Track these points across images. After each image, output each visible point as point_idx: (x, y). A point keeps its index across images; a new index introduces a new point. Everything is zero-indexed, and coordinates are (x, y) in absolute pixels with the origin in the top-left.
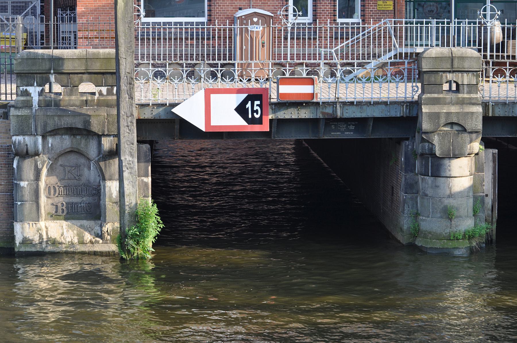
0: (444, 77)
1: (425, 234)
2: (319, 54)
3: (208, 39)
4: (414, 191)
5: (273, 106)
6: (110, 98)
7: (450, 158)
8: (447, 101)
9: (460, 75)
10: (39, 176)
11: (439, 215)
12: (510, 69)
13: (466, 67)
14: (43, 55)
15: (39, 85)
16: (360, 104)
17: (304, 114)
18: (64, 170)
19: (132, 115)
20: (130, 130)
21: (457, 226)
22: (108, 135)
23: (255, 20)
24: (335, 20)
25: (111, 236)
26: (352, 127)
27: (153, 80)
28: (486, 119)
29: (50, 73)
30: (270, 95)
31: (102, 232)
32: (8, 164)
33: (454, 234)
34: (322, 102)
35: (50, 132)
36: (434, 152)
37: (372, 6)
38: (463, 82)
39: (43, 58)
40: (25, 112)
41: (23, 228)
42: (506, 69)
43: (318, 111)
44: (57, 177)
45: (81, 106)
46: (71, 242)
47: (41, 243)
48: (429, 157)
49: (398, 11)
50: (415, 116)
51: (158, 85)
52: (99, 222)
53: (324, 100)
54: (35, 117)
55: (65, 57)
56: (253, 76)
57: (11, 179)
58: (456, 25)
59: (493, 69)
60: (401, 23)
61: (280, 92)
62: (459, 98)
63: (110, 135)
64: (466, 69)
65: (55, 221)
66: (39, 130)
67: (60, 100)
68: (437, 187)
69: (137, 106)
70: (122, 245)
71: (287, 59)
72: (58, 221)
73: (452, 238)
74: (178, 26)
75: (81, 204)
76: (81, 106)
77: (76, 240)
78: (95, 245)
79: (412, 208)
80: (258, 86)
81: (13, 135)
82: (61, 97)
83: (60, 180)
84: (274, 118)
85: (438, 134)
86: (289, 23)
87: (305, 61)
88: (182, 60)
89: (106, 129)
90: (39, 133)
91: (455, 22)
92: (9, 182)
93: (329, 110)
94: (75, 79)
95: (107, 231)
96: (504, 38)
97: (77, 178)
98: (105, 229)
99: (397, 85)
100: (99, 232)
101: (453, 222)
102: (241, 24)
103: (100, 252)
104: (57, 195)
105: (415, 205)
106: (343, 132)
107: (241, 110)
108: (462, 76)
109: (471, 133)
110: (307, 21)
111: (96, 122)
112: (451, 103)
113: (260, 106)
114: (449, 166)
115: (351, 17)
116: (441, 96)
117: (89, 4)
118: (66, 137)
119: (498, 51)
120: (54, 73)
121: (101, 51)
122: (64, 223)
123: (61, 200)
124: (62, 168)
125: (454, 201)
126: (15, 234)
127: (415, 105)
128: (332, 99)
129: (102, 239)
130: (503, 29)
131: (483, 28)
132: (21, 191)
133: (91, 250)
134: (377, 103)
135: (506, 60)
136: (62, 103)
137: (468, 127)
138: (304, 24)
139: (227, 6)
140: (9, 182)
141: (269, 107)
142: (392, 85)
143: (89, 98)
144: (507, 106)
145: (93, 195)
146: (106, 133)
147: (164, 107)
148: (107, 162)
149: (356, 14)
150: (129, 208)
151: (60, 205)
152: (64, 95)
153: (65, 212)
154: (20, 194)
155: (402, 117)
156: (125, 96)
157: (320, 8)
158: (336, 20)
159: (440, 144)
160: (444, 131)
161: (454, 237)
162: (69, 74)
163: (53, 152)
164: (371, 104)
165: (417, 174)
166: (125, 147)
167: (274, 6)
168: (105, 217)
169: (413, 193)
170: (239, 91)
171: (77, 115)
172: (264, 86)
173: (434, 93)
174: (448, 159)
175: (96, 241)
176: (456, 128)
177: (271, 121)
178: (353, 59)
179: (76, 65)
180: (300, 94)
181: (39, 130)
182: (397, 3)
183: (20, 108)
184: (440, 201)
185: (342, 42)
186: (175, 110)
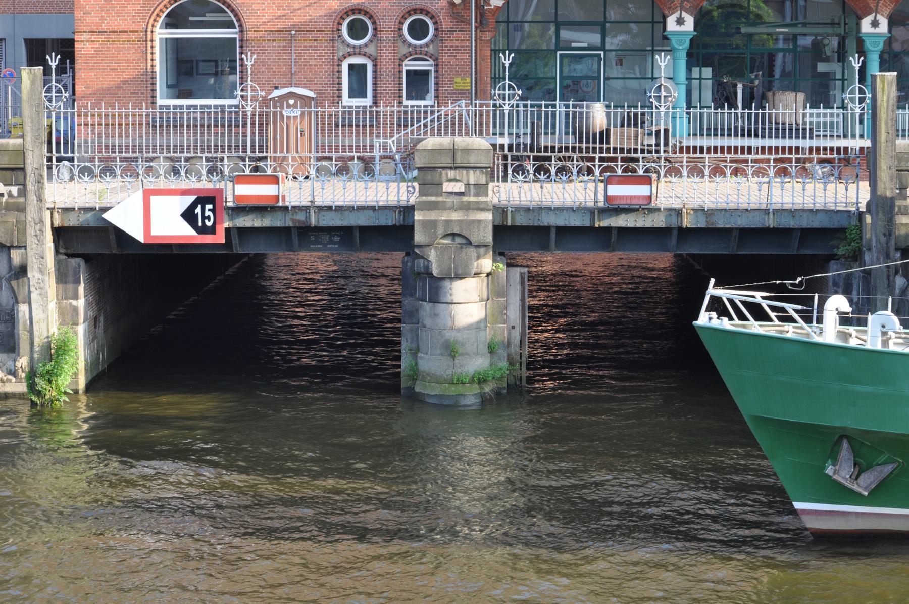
1: (423, 376)
3: (216, 126)
4: (414, 321)
5: (230, 212)
7: (451, 278)
8: (448, 206)
9: (465, 172)
11: (439, 352)
16: (339, 209)
20: (39, 241)
21: (461, 366)
23: (292, 102)
25: (26, 372)
26: (337, 239)
27: (166, 178)
30: (226, 198)
34: (292, 207)
36: (430, 271)
37: (447, 84)
42: (791, 167)
49: (481, 90)
52: (13, 355)
53: (293, 204)
56: (291, 172)
58: (478, 108)
59: (512, 165)
60: (488, 105)
61: (236, 193)
62: (463, 202)
64: (472, 165)
68: (436, 315)
69: (60, 211)
70: (32, 386)
71: (246, 152)
73: (455, 381)
74: (69, 110)
78: (7, 384)
79: (411, 342)
84: (231, 226)
85: (436, 248)
86: (506, 105)
88: (115, 152)
89: (15, 239)
91: (476, 104)
93: (301, 217)
95: (22, 367)
96: (609, 124)
98: (18, 365)
99: (388, 185)
101: (456, 361)
102: (275, 107)
103: (12, 394)
105: (415, 339)
107: (189, 215)
108: (468, 174)
109: (478, 246)
112: (453, 208)
113: (213, 211)
114: (451, 289)
116: (440, 199)
117: (90, 82)
119: (601, 142)
127: (408, 210)
128: (305, 202)
129: (15, 377)
130: (608, 114)
131: (498, 112)
137: (474, 239)
139: (263, 84)
141: (225, 212)
142: (381, 186)
144: (531, 212)
145: (6, 322)
146: (15, 244)
147: (93, 212)
148: (21, 280)
155: (395, 226)
156: (32, 197)
157: (381, 87)
158: (402, 103)
159: (439, 261)
160: (443, 244)
164: (354, 209)
166: (32, 262)
167: (322, 84)
168: (19, 350)
169: (413, 323)
172: (217, 187)
174: (449, 280)
175: (7, 379)
176: (458, 240)
177: (228, 230)
180: (262, 196)
182: (480, 80)
186: (106, 216)
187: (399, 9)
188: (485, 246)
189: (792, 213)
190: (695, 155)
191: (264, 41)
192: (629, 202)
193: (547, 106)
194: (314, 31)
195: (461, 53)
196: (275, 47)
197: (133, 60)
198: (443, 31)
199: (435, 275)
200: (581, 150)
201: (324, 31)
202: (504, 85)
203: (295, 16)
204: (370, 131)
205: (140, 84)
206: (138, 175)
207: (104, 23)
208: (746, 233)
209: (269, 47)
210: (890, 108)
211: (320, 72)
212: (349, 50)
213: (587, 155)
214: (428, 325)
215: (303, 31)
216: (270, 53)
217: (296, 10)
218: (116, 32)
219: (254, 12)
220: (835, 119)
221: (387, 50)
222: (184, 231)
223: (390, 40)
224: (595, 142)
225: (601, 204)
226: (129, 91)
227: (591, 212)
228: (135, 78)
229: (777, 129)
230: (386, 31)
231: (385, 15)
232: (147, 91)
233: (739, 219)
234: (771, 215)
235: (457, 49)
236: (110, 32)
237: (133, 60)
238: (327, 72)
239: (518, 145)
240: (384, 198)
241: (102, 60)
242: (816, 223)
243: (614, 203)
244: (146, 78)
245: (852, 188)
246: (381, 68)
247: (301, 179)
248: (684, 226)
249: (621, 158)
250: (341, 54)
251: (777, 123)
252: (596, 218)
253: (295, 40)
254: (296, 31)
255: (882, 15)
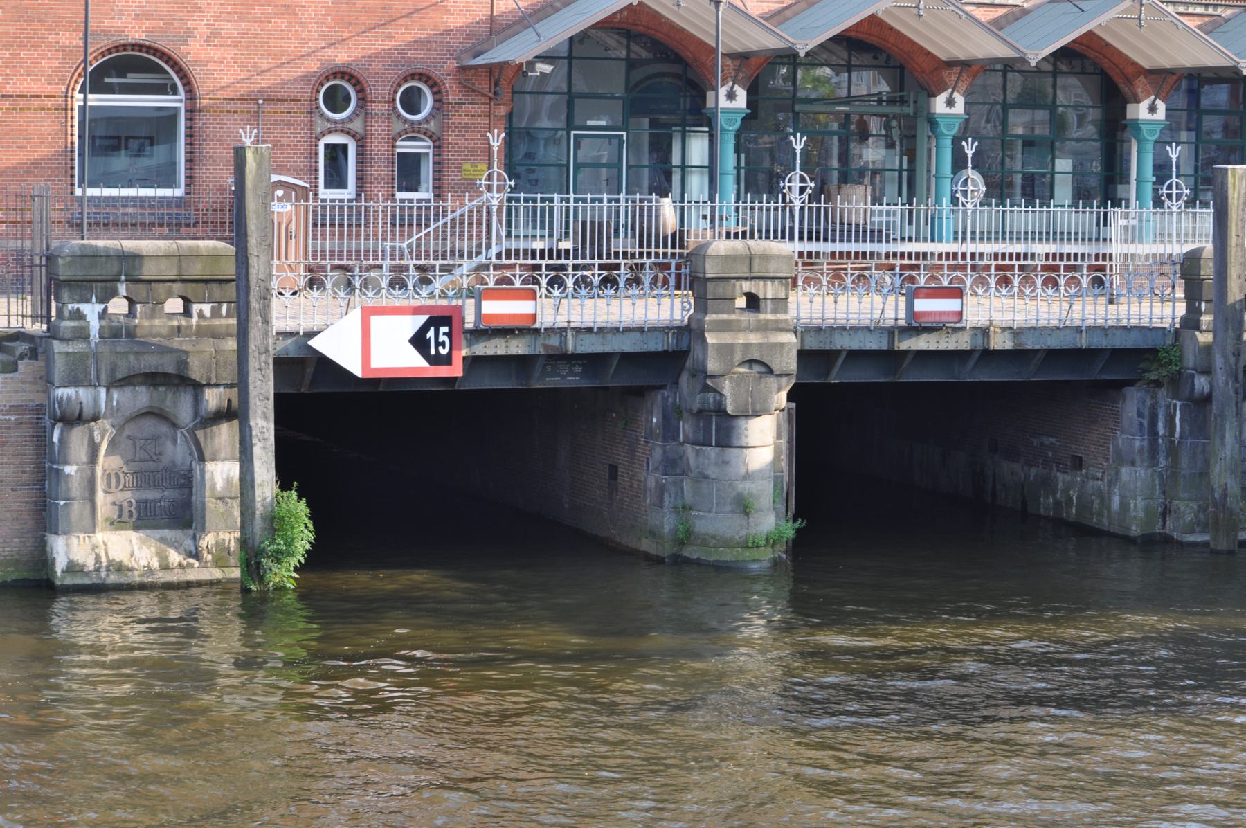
0: (738, 287)
2: (383, 251)
4: (678, 471)
6: (217, 322)
7: (747, 416)
9: (761, 283)
10: (96, 456)
11: (728, 508)
12: (547, 276)
13: (772, 270)
14: (106, 249)
15: (100, 301)
17: (516, 347)
18: (134, 445)
19: (267, 351)
20: (264, 376)
22: (217, 385)
23: (280, 193)
24: (393, 195)
25: (212, 554)
26: (578, 369)
28: (803, 355)
29: (119, 281)
31: (196, 549)
32: (37, 436)
33: (754, 538)
34: (545, 329)
35: (121, 380)
36: (723, 407)
38: (765, 294)
39: (107, 256)
40: (77, 347)
41: (68, 545)
43: (537, 342)
44: (122, 457)
45: (170, 337)
46: (148, 566)
47: (97, 570)
48: (711, 416)
50: (685, 349)
51: (287, 301)
52: (191, 532)
54: (96, 355)
55: (145, 254)
57: (41, 463)
62: (759, 321)
63: (219, 385)
64: (771, 275)
65: (118, 532)
66: (103, 377)
67: (136, 326)
68: (726, 463)
72: (123, 532)
73: (750, 545)
75: (160, 501)
76: (170, 337)
77: (155, 564)
78: (188, 571)
80: (444, 302)
81: (58, 387)
82: (137, 321)
83: (126, 463)
85: (731, 379)
87: (518, 262)
89: (213, 376)
90: (103, 383)
92: (38, 467)
93: (554, 341)
94: (160, 291)
97: (155, 458)
98: (203, 544)
100: (193, 549)
101: (751, 520)
104: (121, 487)
106: (563, 377)
107: (419, 341)
108: (765, 286)
110: (346, 197)
111: (196, 363)
112: (749, 329)
113: (449, 334)
114: (746, 429)
115: (416, 190)
116: (733, 317)
118: (142, 390)
120: (126, 280)
121: (201, 243)
122: (133, 535)
123: (127, 497)
124: (130, 442)
125: (753, 486)
126: (55, 555)
127: (690, 333)
129: (198, 560)
132: (66, 482)
133: (181, 579)
134: (628, 330)
135: (1058, 262)
136: (138, 332)
137: (776, 367)
138: (341, 200)
139: (220, 169)
140: (38, 467)
141: (463, 336)
143: (183, 323)
145: (181, 486)
146: (214, 381)
147: (294, 338)
148: (208, 430)
149: (423, 186)
150: (262, 505)
151: (125, 504)
152: (141, 318)
153: (135, 516)
154: (62, 487)
155: (665, 352)
160: (740, 373)
161: (753, 543)
162: (150, 281)
163: (120, 414)
165: (682, 444)
166: (255, 404)
170: (417, 311)
171: (167, 352)
173: (723, 312)
175: (188, 563)
176: (757, 368)
178: (592, 258)
179: (163, 267)
180: (515, 315)
181: (103, 377)
183: (69, 340)
184: (730, 485)
185: (419, 231)
187: (395, 74)
188: (788, 375)
189: (1105, 330)
190: (1004, 263)
191: (223, 112)
192: (937, 319)
193: (526, 200)
194: (286, 100)
195: (472, 132)
196: (236, 120)
197: (49, 134)
198: (449, 103)
199: (730, 412)
200: (657, 255)
201: (300, 100)
202: (1171, 183)
203: (263, 79)
204: (357, 231)
205: (57, 168)
206: (381, 289)
207: (9, 83)
208: (1053, 355)
209: (229, 120)
210: (1241, 207)
211: (294, 154)
212: (329, 126)
213: (886, 262)
214: (713, 476)
215: (273, 100)
216: (229, 128)
217: (263, 71)
218: (26, 96)
219: (209, 73)
220: (891, 218)
221: (379, 126)
222: (411, 361)
223: (383, 114)
224: (665, 246)
225: (902, 323)
226: (42, 176)
227: (891, 332)
228: (50, 159)
229: (849, 231)
230: (379, 102)
231: (377, 82)
232: (66, 176)
233: (1049, 338)
234: (1084, 334)
235: (466, 126)
236: (17, 96)
237: (49, 134)
238: (302, 154)
239: (551, 251)
240: (1045, 316)
241: (6, 134)
242: (1129, 342)
243: (921, 320)
244: (66, 160)
245: (866, 299)
246: (371, 150)
247: (288, 294)
248: (992, 348)
249: (599, 265)
250: (319, 130)
251: (842, 223)
252: (896, 338)
253: (263, 112)
254: (264, 100)
255: (958, 92)
